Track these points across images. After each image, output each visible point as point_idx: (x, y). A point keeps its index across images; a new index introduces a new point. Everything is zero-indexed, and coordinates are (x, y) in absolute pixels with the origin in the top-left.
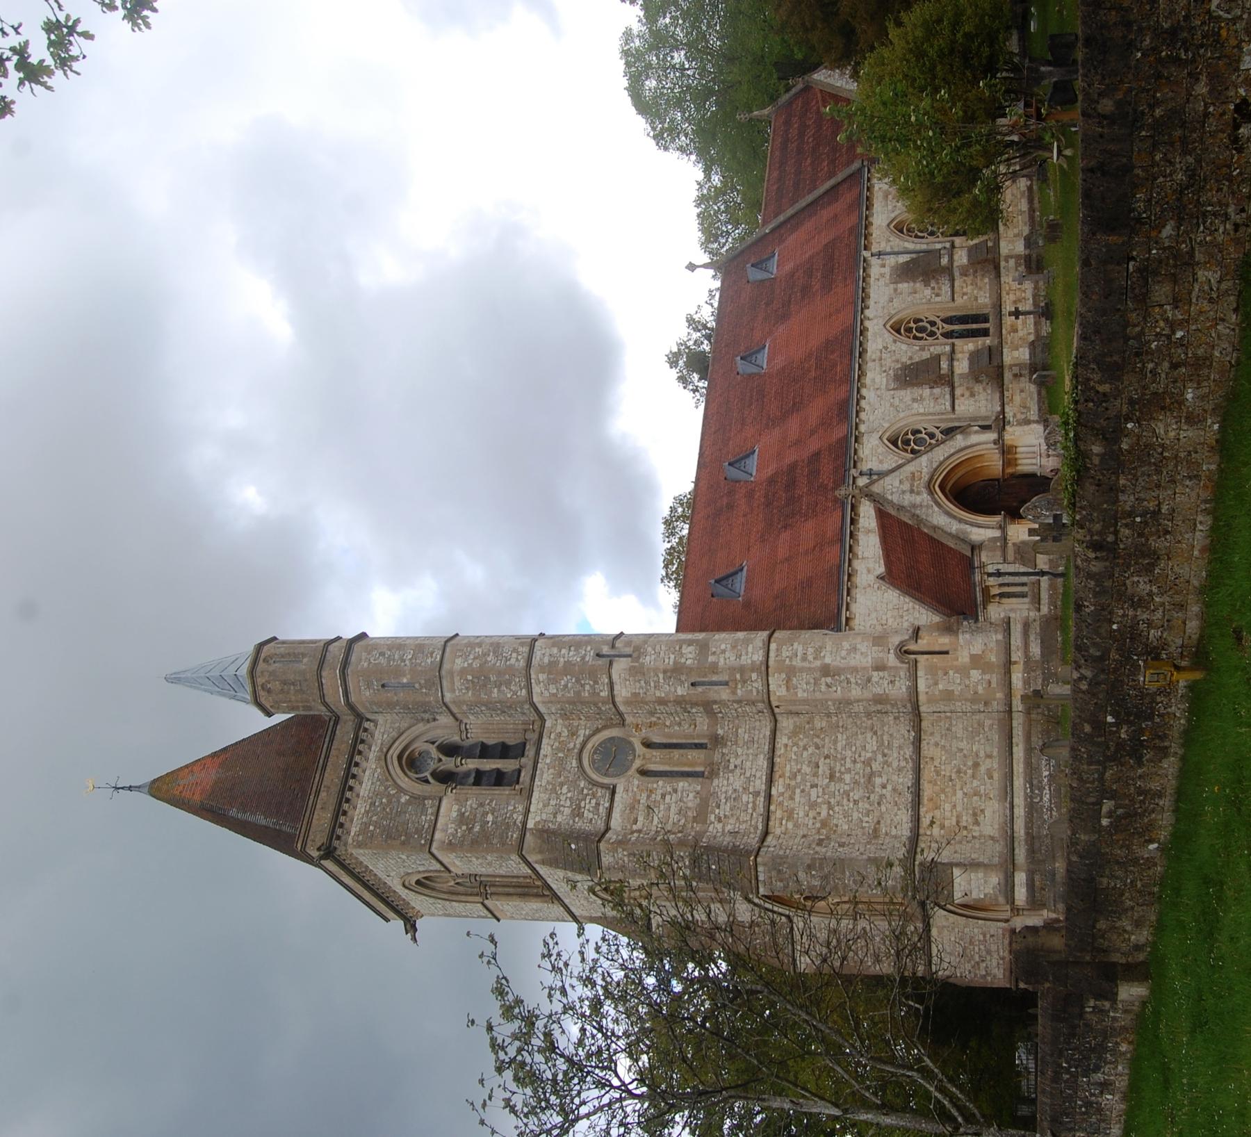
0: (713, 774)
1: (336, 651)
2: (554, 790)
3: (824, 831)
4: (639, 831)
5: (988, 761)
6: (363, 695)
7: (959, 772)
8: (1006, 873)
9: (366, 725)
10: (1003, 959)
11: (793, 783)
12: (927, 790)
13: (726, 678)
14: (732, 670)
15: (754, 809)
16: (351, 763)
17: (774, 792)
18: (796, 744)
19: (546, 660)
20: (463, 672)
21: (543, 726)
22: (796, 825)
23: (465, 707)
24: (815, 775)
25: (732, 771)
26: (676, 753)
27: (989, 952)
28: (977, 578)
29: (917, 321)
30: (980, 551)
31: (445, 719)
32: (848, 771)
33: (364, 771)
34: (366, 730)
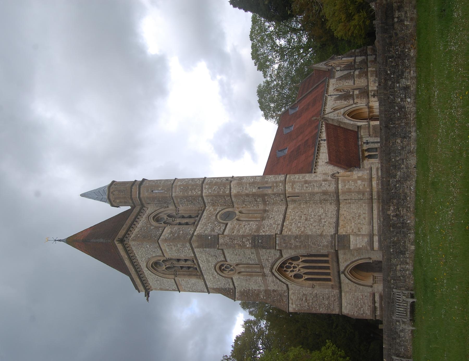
0: (263, 219)
2: (206, 225)
6: (145, 194)
7: (353, 218)
8: (370, 237)
9: (144, 208)
10: (370, 306)
12: (341, 223)
13: (270, 185)
14: (273, 182)
15: (277, 229)
17: (285, 224)
20: (180, 186)
21: (205, 208)
23: (179, 200)
24: (301, 219)
27: (364, 303)
28: (360, 143)
30: (361, 129)
31: (171, 207)
32: (313, 218)
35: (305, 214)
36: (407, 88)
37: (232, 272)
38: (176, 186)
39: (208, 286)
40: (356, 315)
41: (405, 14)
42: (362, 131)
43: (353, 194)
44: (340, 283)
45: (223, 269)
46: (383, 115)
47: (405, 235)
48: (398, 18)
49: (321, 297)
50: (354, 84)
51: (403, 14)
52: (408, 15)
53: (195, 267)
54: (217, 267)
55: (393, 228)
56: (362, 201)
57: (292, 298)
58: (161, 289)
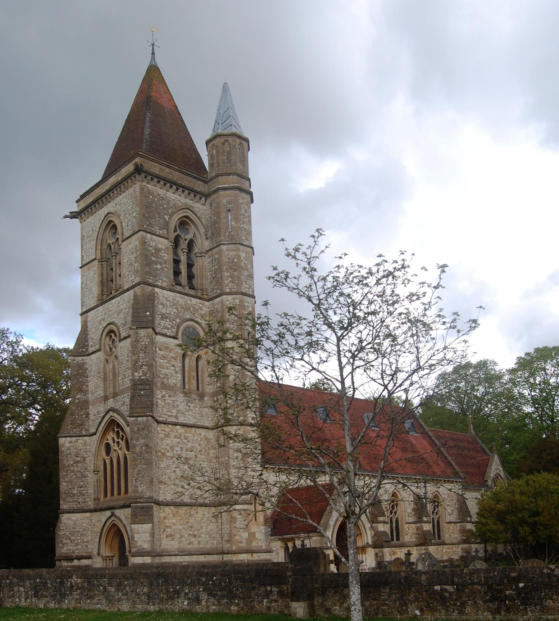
0: (186, 394)
1: (245, 186)
3: (160, 454)
4: (156, 352)
5: (197, 542)
6: (224, 198)
7: (191, 527)
8: (150, 552)
9: (203, 199)
10: (73, 552)
11: (183, 438)
15: (169, 416)
16: (184, 188)
17: (178, 427)
18: (201, 440)
19: (246, 304)
20: (239, 257)
22: (162, 439)
23: (216, 256)
24: (187, 450)
25: (187, 405)
26: (194, 374)
27: (77, 545)
28: (302, 535)
29: (397, 505)
31: (207, 244)
33: (180, 195)
34: (201, 198)
35: (196, 456)
36: (198, 600)
37: (108, 349)
38: (238, 250)
39: (89, 313)
40: (60, 533)
41: (274, 600)
42: (318, 538)
43: (228, 526)
44: (101, 510)
45: (111, 336)
46: (171, 571)
47: (53, 597)
48: (271, 590)
49: (82, 483)
50: (448, 523)
51: (275, 597)
52: (273, 604)
53: (113, 292)
54: (112, 327)
55: (60, 582)
56: (220, 539)
57: (79, 441)
58: (82, 237)
